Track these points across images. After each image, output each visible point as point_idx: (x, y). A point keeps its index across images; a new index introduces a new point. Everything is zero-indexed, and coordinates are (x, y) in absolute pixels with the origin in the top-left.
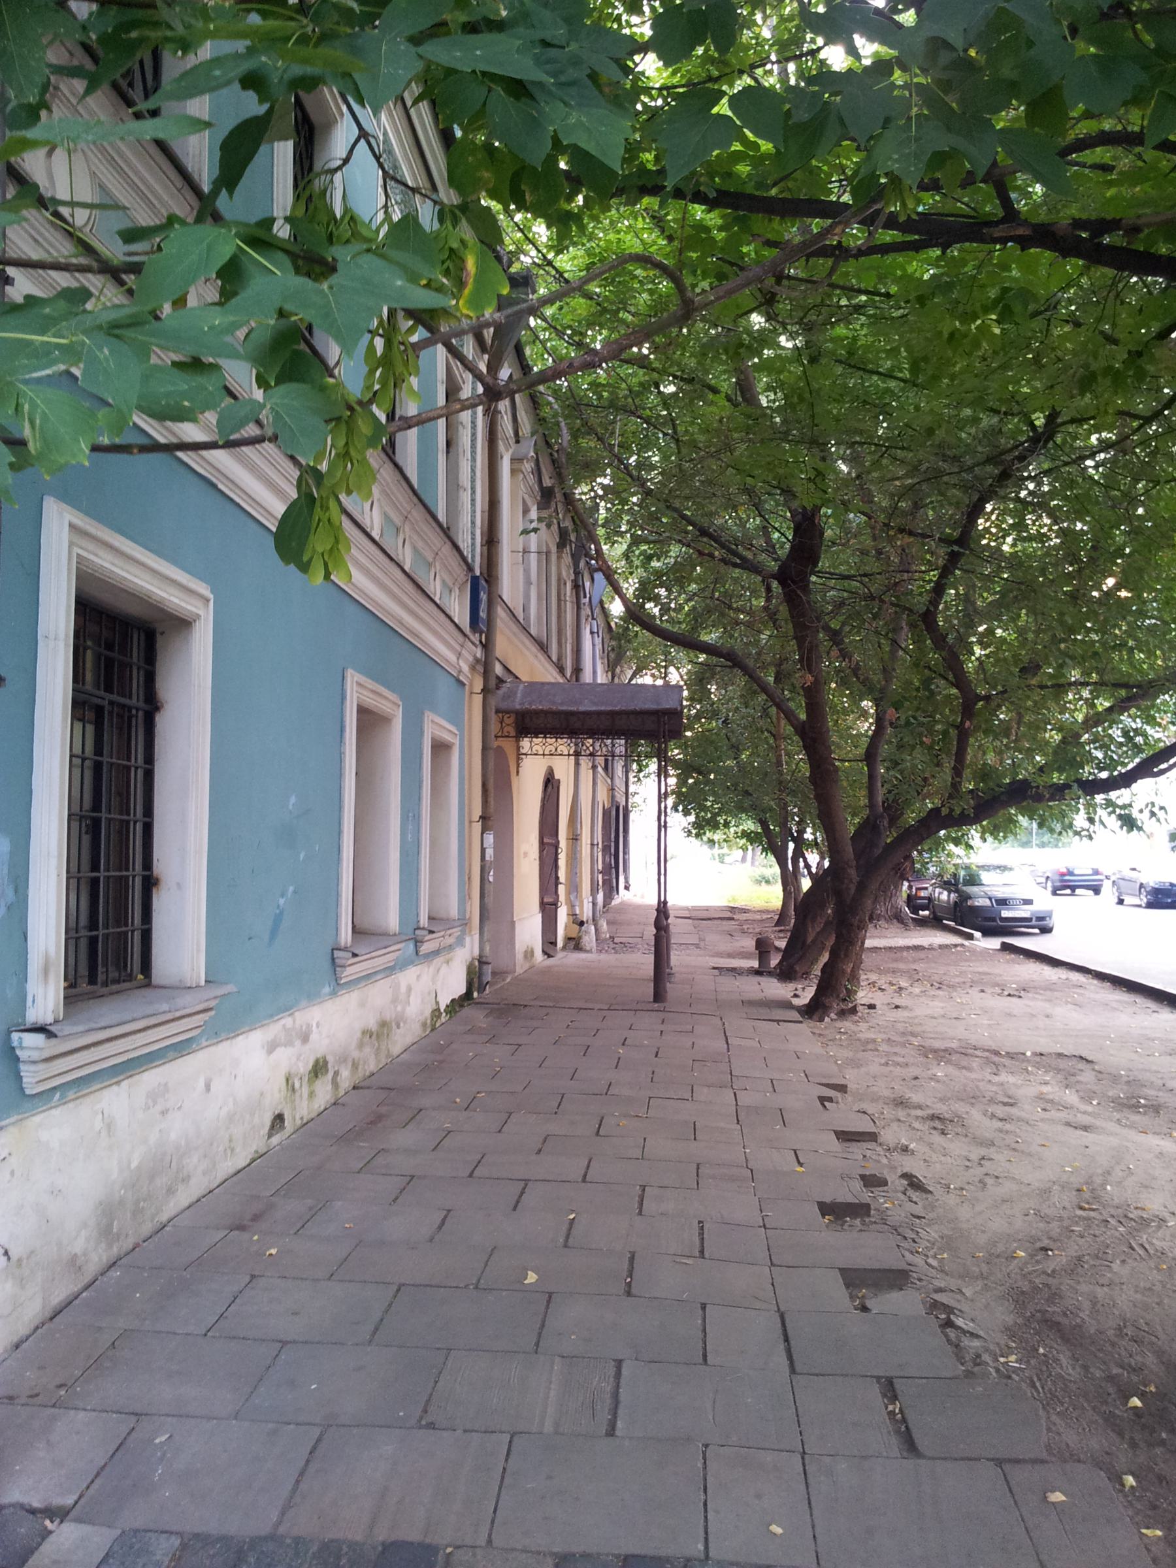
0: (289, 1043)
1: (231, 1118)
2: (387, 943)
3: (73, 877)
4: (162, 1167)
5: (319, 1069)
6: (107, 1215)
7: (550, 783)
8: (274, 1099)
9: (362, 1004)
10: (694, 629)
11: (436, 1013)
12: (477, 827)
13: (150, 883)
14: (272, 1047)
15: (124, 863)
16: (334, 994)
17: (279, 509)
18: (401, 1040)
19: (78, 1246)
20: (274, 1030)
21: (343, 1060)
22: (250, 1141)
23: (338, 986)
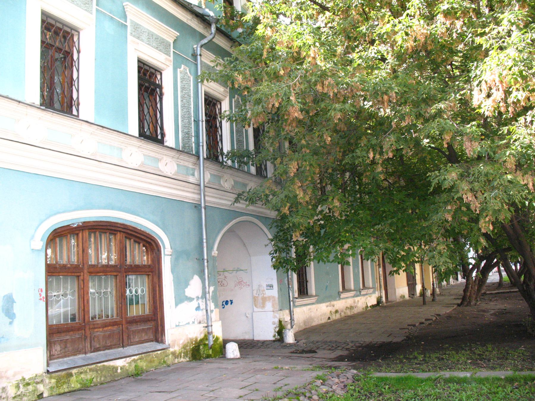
0: (330, 306)
1: (321, 316)
2: (210, 268)
3: (298, 281)
4: (311, 319)
5: (337, 312)
6: (305, 322)
7: (61, 257)
8: (328, 315)
9: (346, 302)
10: (108, 262)
11: (367, 307)
12: (378, 267)
13: (307, 282)
14: (327, 306)
15: (303, 279)
16: (339, 300)
17: (93, 263)
18: (356, 311)
19: (301, 324)
20: (328, 304)
21: (342, 311)
22: (324, 320)
23: (340, 299)
